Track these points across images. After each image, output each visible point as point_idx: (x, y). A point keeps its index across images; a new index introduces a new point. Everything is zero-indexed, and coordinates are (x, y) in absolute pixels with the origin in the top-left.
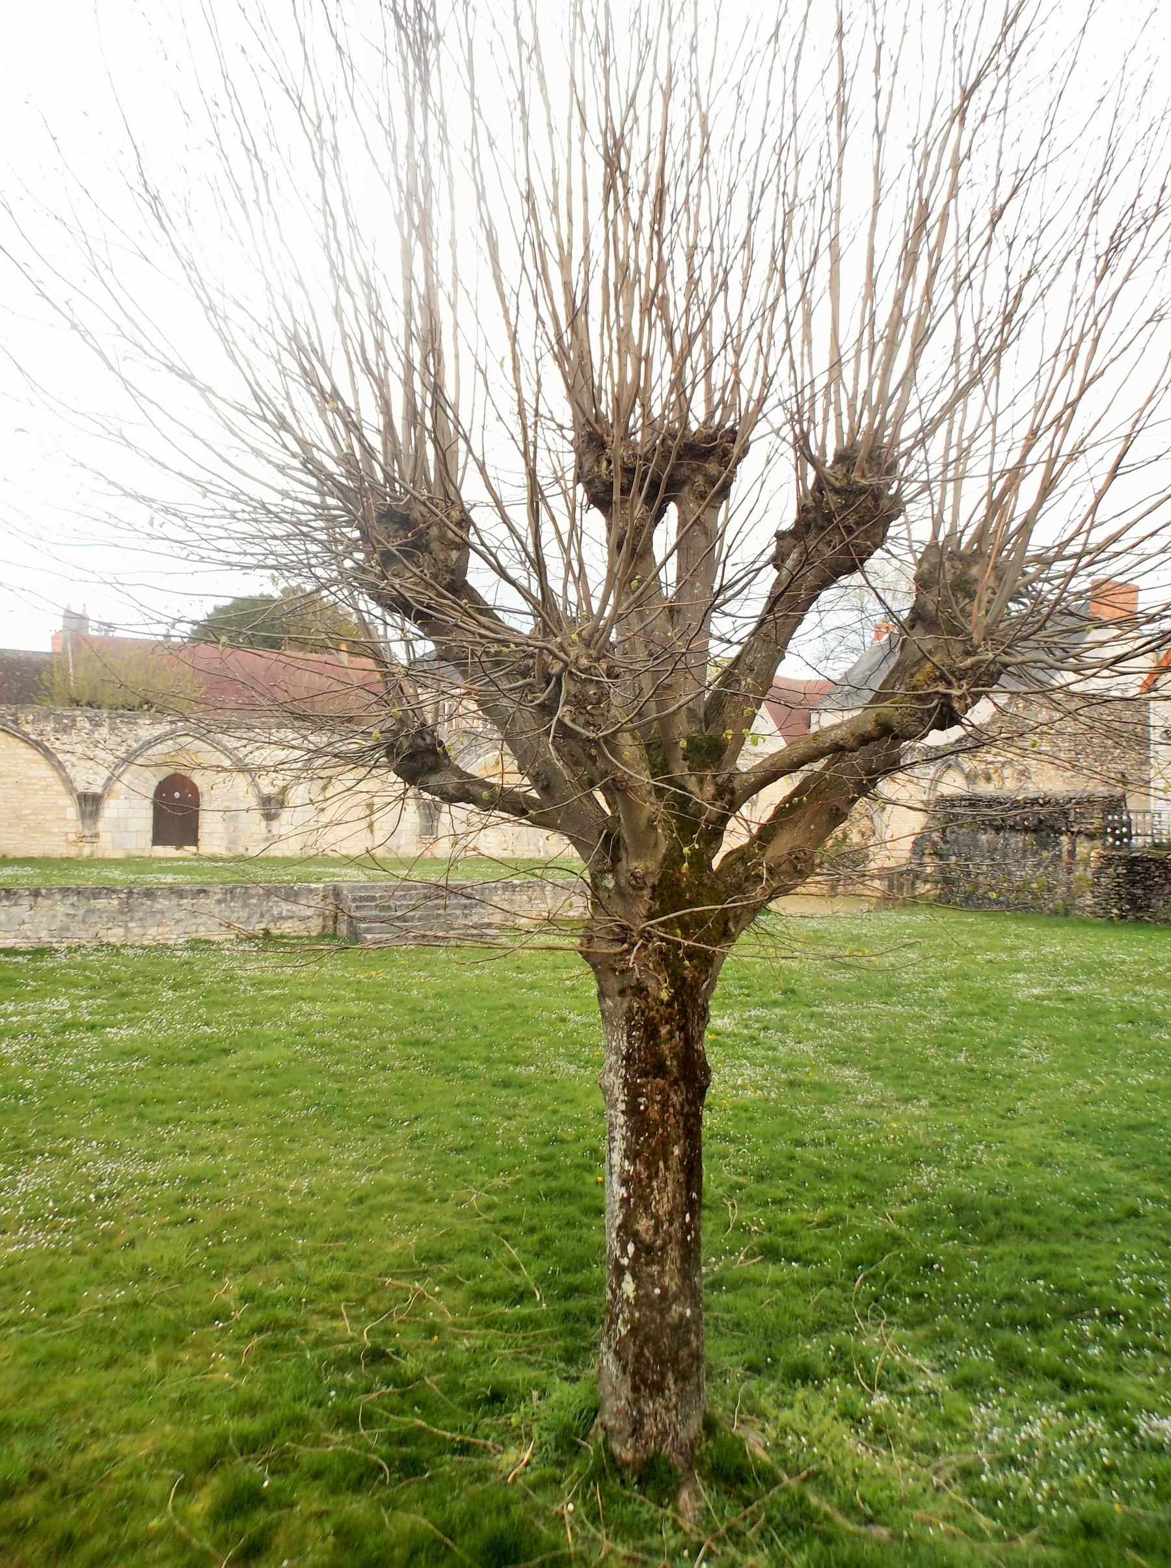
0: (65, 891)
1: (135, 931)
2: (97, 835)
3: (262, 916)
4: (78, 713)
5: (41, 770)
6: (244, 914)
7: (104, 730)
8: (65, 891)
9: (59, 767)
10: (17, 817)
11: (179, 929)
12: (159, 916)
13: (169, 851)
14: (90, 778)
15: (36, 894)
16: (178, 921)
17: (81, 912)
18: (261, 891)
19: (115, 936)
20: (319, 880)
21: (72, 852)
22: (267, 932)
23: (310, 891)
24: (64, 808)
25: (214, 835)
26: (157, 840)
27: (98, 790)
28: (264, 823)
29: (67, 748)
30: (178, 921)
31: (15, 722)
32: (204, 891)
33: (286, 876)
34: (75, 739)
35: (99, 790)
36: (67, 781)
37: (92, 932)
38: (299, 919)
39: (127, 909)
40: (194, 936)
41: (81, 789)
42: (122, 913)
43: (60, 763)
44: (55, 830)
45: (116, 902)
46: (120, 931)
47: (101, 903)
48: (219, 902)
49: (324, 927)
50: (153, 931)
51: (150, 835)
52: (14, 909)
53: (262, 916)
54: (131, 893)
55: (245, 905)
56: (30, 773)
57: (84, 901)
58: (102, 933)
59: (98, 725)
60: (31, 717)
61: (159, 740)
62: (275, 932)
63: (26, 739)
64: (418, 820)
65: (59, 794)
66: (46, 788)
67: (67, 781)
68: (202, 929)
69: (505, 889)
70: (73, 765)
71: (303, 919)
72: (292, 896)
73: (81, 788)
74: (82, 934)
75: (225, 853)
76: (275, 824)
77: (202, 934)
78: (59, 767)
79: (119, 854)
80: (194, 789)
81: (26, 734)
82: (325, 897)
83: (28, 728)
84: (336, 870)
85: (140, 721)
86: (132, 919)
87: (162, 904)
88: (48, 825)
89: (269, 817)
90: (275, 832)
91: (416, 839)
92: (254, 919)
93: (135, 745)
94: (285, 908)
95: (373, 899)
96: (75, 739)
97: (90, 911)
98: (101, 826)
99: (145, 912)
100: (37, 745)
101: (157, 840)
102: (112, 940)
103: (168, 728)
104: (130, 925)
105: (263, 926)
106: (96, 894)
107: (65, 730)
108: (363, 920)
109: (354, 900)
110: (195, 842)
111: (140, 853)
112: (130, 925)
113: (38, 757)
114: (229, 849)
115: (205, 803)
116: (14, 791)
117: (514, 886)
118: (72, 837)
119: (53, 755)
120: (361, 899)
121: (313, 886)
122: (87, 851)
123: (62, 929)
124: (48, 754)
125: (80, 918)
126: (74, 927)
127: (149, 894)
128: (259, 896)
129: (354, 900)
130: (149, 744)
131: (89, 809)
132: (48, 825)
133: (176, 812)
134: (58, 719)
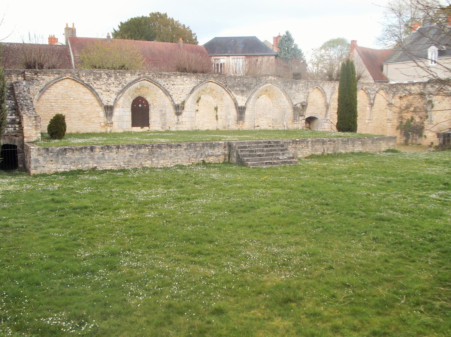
0: (129, 146)
1: (155, 162)
2: (112, 123)
3: (202, 155)
4: (102, 71)
5: (89, 96)
6: (195, 154)
7: (113, 79)
8: (129, 146)
9: (96, 95)
10: (82, 116)
11: (171, 161)
12: (163, 156)
13: (138, 129)
14: (108, 99)
15: (118, 147)
16: (171, 157)
17: (135, 154)
18: (201, 145)
19: (148, 164)
20: (220, 140)
21: (103, 130)
22: (204, 161)
23: (219, 144)
24: (99, 112)
25: (155, 123)
26: (134, 125)
27: (111, 104)
28: (176, 117)
29: (99, 87)
30: (171, 157)
31: (78, 76)
32: (180, 145)
33: (208, 137)
34: (102, 83)
35: (112, 104)
36: (100, 101)
37: (139, 163)
38: (217, 154)
39: (152, 153)
40: (177, 163)
41: (105, 104)
42: (150, 155)
43: (97, 93)
44: (96, 121)
45: (147, 150)
46: (149, 162)
47: (142, 151)
48: (185, 149)
49: (225, 159)
50: (162, 162)
51: (131, 123)
52: (110, 154)
53: (202, 155)
54: (153, 146)
55: (195, 151)
56: (85, 98)
57: (136, 150)
58: (143, 163)
59: (110, 76)
60: (84, 74)
61: (134, 82)
62: (207, 162)
63: (83, 84)
64: (236, 114)
65: (97, 106)
66: (91, 104)
67: (100, 101)
68: (179, 161)
69: (293, 143)
70: (102, 94)
71: (217, 156)
72: (212, 146)
73: (105, 103)
74: (136, 163)
75: (161, 130)
76: (180, 117)
77: (180, 163)
78: (96, 95)
79: (120, 131)
80: (147, 103)
81: (83, 81)
82: (225, 147)
83: (83, 79)
84: (225, 136)
85: (127, 75)
86: (154, 157)
87: (165, 150)
88: (93, 119)
89: (178, 114)
90: (180, 120)
91: (235, 122)
92: (199, 157)
93: (125, 85)
94: (210, 151)
95: (246, 147)
96: (102, 83)
97: (138, 154)
98: (114, 119)
99: (158, 154)
100: (87, 86)
101: (134, 125)
102: (147, 166)
103: (137, 77)
104: (153, 159)
105: (202, 159)
106: (140, 147)
107: (98, 79)
108: (245, 156)
109: (239, 148)
110: (148, 125)
111: (128, 130)
112: (153, 159)
113: (88, 91)
114: (162, 128)
115: (151, 108)
116: (79, 106)
117: (297, 141)
118: (103, 124)
119: (94, 90)
120: (242, 147)
121: (220, 142)
122: (109, 130)
123: (128, 162)
124: (92, 90)
125: (135, 157)
126: (133, 160)
127: (159, 147)
128: (200, 147)
129: (239, 148)
130: (130, 84)
131: (109, 112)
132: (93, 119)
133: (140, 112)
134: (95, 74)
